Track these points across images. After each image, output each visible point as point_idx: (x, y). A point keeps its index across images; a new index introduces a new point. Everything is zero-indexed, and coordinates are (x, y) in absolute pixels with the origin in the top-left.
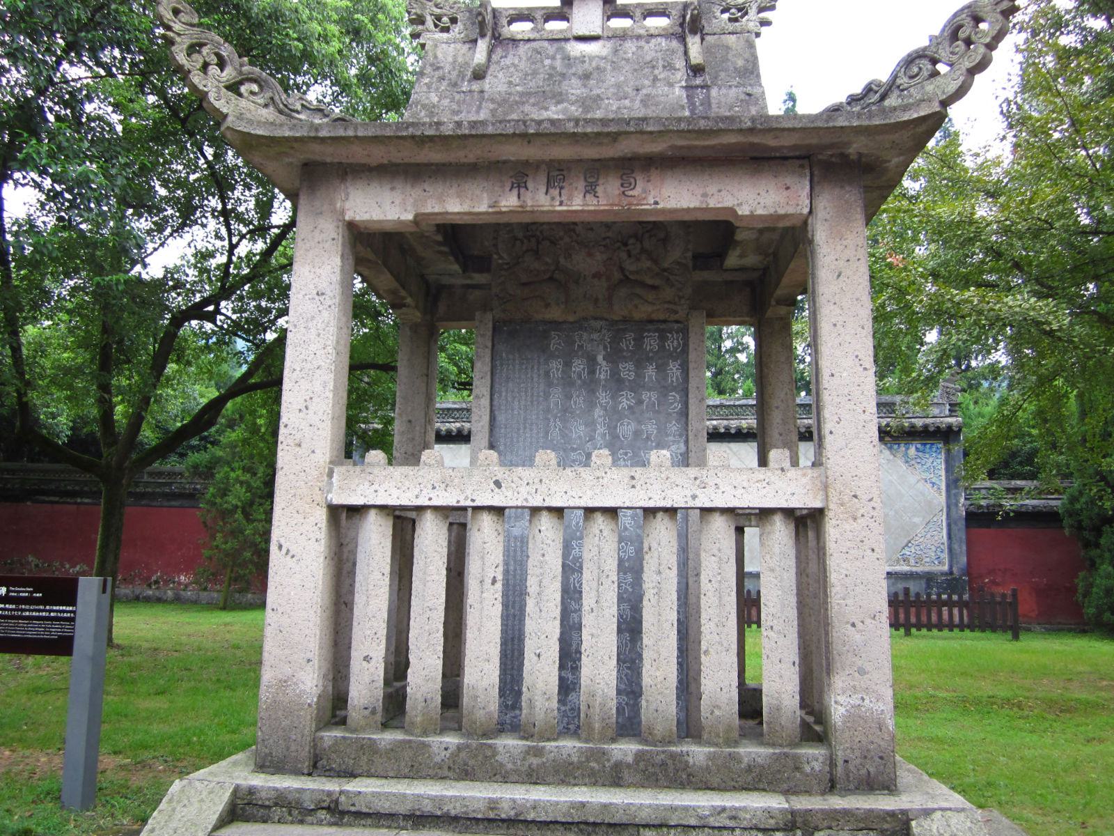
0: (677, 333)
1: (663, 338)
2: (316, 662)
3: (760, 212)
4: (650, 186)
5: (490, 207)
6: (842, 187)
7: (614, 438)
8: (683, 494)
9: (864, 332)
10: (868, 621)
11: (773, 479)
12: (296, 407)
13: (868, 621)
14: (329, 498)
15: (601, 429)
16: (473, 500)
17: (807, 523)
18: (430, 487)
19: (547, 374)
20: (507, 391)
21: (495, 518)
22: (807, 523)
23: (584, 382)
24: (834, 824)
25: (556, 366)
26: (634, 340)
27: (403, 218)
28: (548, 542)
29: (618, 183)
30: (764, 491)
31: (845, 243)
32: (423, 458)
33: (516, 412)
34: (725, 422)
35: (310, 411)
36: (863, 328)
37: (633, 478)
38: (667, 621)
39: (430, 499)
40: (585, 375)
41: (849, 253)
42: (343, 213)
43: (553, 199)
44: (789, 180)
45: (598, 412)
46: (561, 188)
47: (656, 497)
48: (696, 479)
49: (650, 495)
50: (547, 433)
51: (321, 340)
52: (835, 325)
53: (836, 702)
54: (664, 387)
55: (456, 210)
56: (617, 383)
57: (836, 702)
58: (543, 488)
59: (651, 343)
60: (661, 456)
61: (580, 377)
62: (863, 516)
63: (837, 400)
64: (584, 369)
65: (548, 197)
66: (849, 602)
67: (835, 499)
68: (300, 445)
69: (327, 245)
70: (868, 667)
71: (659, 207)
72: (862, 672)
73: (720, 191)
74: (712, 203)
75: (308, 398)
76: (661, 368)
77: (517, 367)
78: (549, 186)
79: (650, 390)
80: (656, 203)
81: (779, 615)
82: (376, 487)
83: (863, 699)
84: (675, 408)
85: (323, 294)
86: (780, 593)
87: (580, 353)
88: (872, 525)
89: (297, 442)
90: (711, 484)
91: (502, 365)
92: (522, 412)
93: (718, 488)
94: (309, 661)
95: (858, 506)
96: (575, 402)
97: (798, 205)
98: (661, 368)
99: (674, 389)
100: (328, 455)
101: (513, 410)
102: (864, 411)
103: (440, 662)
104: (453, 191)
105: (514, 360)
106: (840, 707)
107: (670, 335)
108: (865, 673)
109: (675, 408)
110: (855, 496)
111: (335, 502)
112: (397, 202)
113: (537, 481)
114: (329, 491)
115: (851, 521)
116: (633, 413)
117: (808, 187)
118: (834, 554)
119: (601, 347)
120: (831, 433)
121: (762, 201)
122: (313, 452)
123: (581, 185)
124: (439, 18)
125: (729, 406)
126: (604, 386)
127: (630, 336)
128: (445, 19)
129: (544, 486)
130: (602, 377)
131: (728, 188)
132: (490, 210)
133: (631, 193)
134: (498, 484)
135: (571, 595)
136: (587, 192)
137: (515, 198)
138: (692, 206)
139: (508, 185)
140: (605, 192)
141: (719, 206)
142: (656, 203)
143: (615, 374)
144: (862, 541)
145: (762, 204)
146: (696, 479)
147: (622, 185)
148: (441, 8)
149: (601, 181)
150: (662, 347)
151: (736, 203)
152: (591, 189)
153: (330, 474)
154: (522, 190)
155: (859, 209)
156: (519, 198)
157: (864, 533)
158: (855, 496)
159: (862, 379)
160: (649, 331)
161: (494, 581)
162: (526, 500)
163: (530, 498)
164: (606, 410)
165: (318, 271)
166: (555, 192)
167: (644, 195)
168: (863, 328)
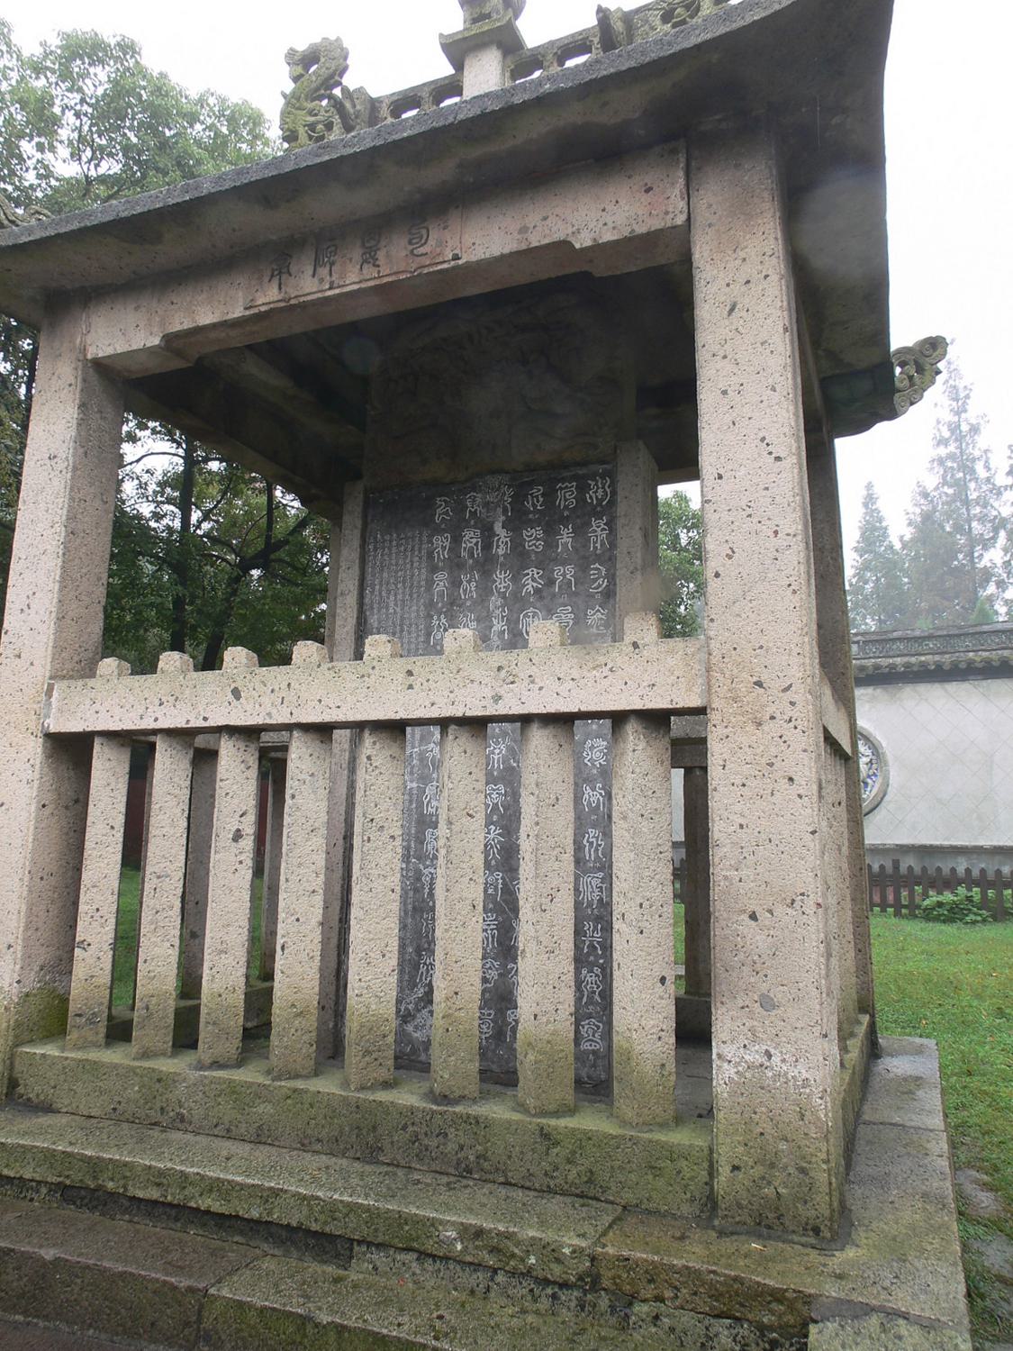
0: (603, 478)
1: (583, 488)
2: (19, 948)
3: (608, 236)
4: (447, 235)
5: (246, 309)
6: (737, 166)
7: (515, 636)
8: (479, 696)
9: (776, 397)
10: (780, 910)
11: (619, 661)
12: (18, 606)
13: (780, 910)
14: (46, 725)
15: (498, 626)
16: (205, 719)
17: (680, 737)
18: (157, 702)
19: (430, 555)
20: (381, 585)
21: (241, 745)
22: (680, 737)
23: (476, 561)
24: (668, 1294)
25: (442, 543)
26: (543, 495)
27: (149, 345)
28: (302, 777)
29: (404, 241)
30: (606, 683)
31: (742, 254)
32: (161, 664)
33: (391, 611)
34: (937, 658)
35: (32, 611)
36: (774, 389)
37: (410, 673)
38: (461, 899)
39: (156, 720)
40: (478, 553)
41: (749, 270)
42: (84, 351)
43: (321, 281)
44: (649, 179)
45: (495, 601)
46: (332, 264)
47: (441, 701)
48: (500, 668)
49: (433, 698)
50: (429, 634)
51: (49, 517)
52: (725, 393)
53: (719, 1056)
54: (584, 557)
55: (208, 322)
56: (520, 559)
57: (719, 1056)
58: (290, 697)
59: (567, 496)
60: (459, 638)
61: (471, 555)
62: (772, 718)
63: (726, 517)
64: (476, 544)
65: (316, 280)
66: (744, 873)
67: (723, 691)
68: (19, 657)
69: (64, 394)
70: (778, 994)
71: (460, 262)
72: (767, 1003)
73: (545, 218)
74: (536, 240)
75: (31, 593)
76: (581, 531)
77: (394, 550)
78: (317, 264)
79: (563, 564)
80: (456, 257)
81: (631, 894)
82: (97, 707)
83: (769, 1056)
84: (600, 586)
85: (55, 457)
86: (632, 855)
87: (472, 522)
88: (789, 734)
89: (16, 652)
90: (521, 675)
91: (375, 549)
92: (398, 610)
93: (533, 682)
94: (10, 947)
95: (764, 699)
96: (465, 591)
97: (667, 213)
98: (581, 531)
99: (598, 559)
100: (48, 667)
101: (387, 609)
102: (776, 533)
103: (175, 953)
104: (204, 296)
105: (391, 541)
106: (726, 1065)
107: (593, 483)
108: (774, 1007)
109: (600, 586)
110: (759, 684)
111: (52, 730)
112: (141, 326)
113: (284, 685)
114: (47, 716)
115: (751, 728)
116: (541, 598)
117: (682, 181)
118: (720, 789)
119: (500, 510)
120: (717, 575)
121: (609, 220)
122: (32, 664)
123: (357, 254)
124: (312, 127)
125: (940, 636)
126: (502, 565)
127: (538, 491)
128: (320, 127)
129: (293, 692)
130: (501, 552)
131: (558, 210)
132: (247, 313)
133: (422, 250)
134: (236, 693)
135: (504, 859)
136: (365, 261)
137: (276, 290)
138: (506, 251)
139: (266, 279)
140: (388, 256)
141: (547, 241)
142: (456, 257)
143: (518, 550)
144: (771, 765)
145: (610, 225)
146: (500, 668)
147: (410, 243)
148: (316, 115)
149: (383, 243)
150: (581, 500)
151: (570, 231)
152: (370, 258)
153: (49, 693)
154: (284, 277)
155: (766, 195)
156: (280, 288)
157: (773, 751)
158: (759, 684)
159: (772, 477)
160: (563, 480)
161: (238, 836)
162: (269, 714)
163: (274, 711)
164: (504, 597)
165: (52, 428)
166: (323, 272)
167: (438, 250)
168: (774, 389)
